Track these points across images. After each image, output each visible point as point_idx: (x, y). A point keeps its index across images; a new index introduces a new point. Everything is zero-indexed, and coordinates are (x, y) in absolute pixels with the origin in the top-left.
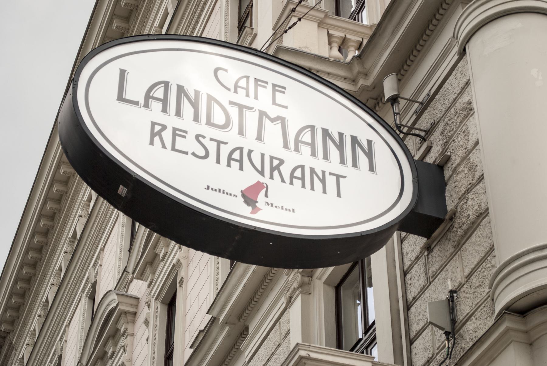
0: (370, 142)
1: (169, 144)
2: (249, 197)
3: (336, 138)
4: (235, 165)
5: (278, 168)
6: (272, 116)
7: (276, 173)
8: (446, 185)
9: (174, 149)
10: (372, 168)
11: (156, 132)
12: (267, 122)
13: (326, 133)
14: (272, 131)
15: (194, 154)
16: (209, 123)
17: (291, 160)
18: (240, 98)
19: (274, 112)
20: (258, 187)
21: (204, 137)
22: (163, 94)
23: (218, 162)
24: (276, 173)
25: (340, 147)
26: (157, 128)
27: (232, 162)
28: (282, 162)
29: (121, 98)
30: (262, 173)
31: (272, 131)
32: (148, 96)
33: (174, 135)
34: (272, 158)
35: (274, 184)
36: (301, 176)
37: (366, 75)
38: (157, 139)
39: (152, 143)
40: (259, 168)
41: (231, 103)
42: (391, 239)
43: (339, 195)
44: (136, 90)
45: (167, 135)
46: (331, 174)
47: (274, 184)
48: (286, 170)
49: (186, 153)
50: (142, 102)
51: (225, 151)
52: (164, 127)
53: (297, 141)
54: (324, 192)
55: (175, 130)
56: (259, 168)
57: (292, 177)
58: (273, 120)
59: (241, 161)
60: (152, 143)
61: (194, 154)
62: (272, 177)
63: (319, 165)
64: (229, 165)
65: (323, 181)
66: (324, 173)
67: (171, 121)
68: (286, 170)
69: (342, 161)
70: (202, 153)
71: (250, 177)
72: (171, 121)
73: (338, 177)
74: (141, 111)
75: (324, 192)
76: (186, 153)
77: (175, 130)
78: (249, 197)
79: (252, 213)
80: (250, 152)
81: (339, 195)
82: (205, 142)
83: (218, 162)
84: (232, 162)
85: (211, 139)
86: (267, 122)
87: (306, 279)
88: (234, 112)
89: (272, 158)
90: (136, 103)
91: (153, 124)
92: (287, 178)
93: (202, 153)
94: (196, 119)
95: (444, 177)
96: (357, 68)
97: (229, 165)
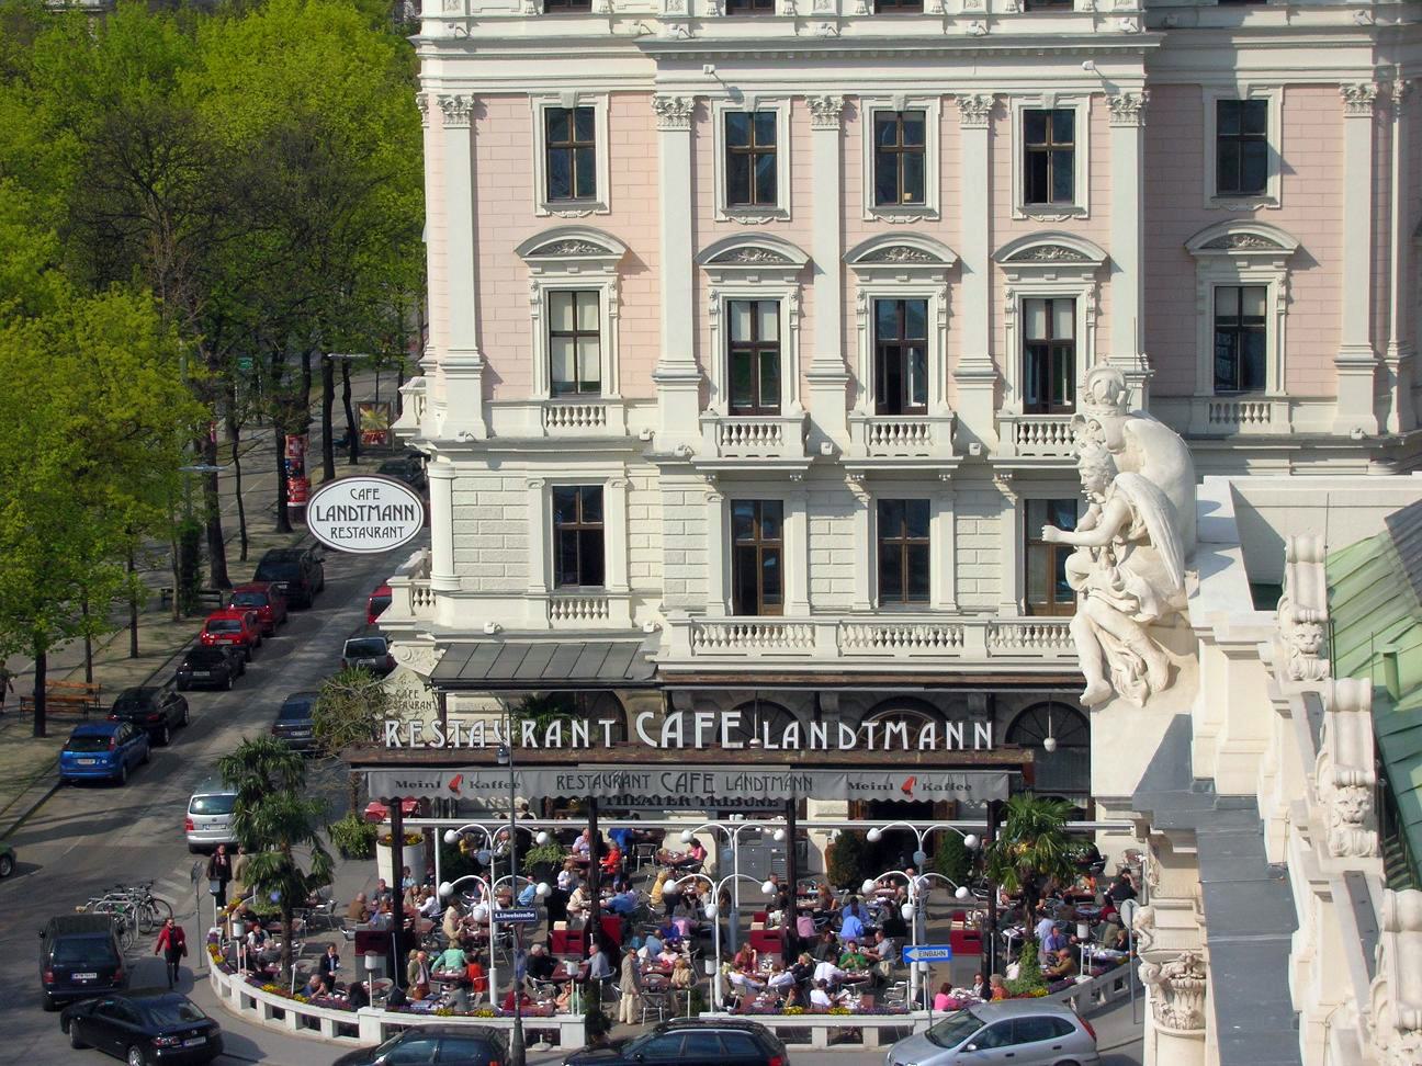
9: (701, 422)
14: (374, 513)
31: (374, 513)
44: (323, 516)
45: (565, 781)
67: (337, 524)
72: (337, 524)
88: (359, 510)
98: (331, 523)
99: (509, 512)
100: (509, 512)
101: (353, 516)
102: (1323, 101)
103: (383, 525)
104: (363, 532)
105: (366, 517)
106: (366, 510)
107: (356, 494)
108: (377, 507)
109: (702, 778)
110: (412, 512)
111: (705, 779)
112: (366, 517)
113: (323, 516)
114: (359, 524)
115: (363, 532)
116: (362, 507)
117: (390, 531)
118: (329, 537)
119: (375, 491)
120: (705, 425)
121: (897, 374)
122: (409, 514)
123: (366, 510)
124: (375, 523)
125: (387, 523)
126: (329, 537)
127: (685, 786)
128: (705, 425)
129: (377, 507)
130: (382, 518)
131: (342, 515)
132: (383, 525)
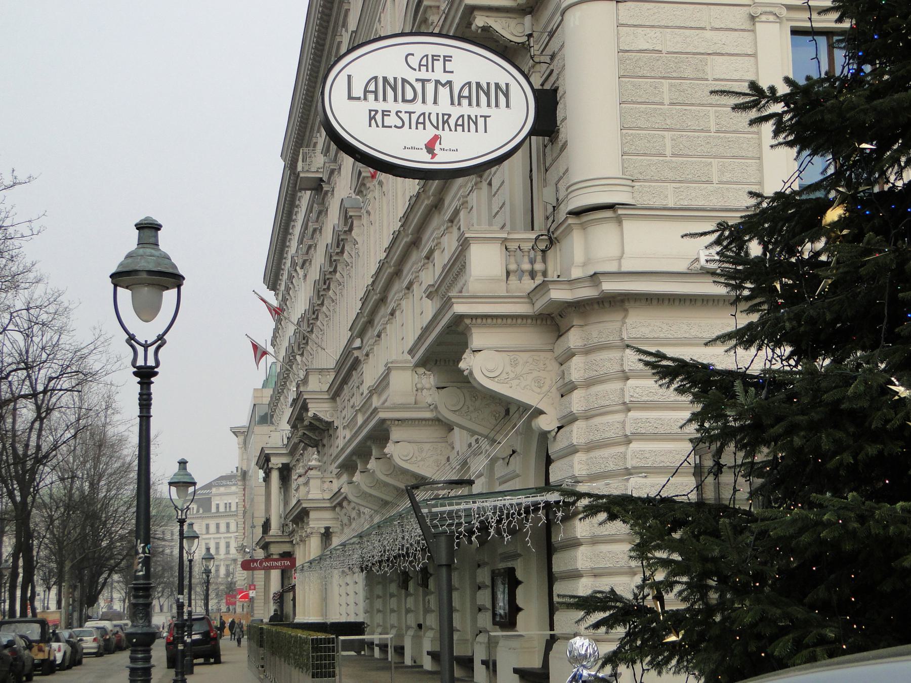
0: (507, 85)
1: (380, 124)
2: (430, 148)
3: (392, 81)
4: (421, 126)
5: (447, 121)
9: (383, 126)
10: (508, 106)
13: (385, 79)
14: (444, 92)
15: (396, 126)
16: (404, 100)
17: (456, 112)
18: (423, 75)
19: (444, 78)
20: (436, 138)
22: (381, 86)
23: (410, 128)
24: (446, 125)
26: (373, 113)
28: (450, 116)
29: (350, 98)
30: (437, 128)
31: (444, 92)
32: (366, 92)
33: (383, 115)
34: (443, 115)
35: (445, 135)
36: (466, 123)
39: (370, 126)
40: (408, 87)
41: (417, 80)
43: (486, 132)
44: (358, 91)
45: (379, 117)
47: (445, 135)
48: (452, 122)
49: (391, 127)
50: (362, 97)
51: (414, 117)
52: (377, 112)
53: (460, 97)
54: (477, 131)
56: (408, 87)
57: (456, 125)
58: (443, 85)
59: (424, 123)
60: (370, 126)
61: (396, 126)
62: (443, 130)
63: (474, 111)
64: (417, 128)
67: (380, 106)
69: (489, 105)
70: (400, 124)
71: (431, 132)
72: (380, 106)
73: (485, 117)
74: (362, 103)
75: (477, 131)
76: (391, 127)
77: (383, 111)
78: (430, 148)
79: (432, 158)
80: (430, 114)
81: (486, 132)
83: (410, 128)
86: (440, 87)
87: (479, 179)
88: (418, 86)
89: (443, 115)
90: (359, 99)
91: (370, 111)
92: (453, 128)
93: (400, 124)
94: (396, 100)
97: (417, 128)
101: (409, 95)
106: (430, 87)
108: (449, 83)
109: (442, 59)
110: (507, 95)
111: (445, 61)
113: (358, 91)
114: (418, 107)
116: (423, 81)
119: (447, 58)
123: (430, 87)
125: (465, 109)
127: (427, 66)
129: (449, 83)
131: (390, 93)
132: (456, 112)
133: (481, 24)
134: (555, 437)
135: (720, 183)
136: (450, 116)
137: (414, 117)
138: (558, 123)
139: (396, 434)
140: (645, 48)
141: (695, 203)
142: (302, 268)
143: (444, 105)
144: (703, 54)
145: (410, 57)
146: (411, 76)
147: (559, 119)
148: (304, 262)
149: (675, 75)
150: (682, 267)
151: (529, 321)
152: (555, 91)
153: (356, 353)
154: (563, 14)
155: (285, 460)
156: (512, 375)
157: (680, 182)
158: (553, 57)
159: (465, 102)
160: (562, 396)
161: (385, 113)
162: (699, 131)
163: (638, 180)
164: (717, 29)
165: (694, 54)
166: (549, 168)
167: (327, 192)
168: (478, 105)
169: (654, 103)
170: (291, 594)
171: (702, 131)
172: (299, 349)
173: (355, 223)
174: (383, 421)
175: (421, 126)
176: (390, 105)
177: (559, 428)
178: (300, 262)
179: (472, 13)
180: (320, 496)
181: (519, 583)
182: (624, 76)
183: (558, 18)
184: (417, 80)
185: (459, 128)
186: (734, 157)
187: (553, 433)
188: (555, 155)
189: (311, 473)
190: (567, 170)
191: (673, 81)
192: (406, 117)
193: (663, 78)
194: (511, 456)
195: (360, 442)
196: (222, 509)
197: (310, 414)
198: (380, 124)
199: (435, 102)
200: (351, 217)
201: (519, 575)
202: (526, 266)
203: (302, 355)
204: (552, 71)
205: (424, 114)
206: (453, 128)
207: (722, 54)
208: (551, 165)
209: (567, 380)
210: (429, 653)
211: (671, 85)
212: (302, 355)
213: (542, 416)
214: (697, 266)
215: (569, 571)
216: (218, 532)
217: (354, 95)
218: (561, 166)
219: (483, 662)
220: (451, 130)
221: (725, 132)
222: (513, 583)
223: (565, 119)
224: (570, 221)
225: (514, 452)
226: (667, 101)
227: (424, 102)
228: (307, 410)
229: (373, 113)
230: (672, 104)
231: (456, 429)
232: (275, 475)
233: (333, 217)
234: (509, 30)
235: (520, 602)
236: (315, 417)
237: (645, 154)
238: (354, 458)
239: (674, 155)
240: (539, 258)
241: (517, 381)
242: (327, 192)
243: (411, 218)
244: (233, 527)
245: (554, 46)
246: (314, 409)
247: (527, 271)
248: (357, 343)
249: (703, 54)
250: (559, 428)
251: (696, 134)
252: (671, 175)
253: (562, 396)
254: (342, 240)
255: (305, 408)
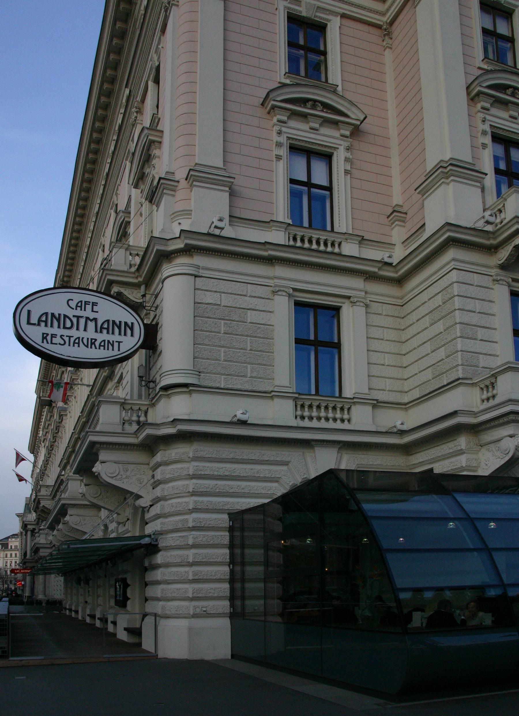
0: (132, 323)
1: (49, 342)
4: (76, 345)
6: (91, 318)
7: (93, 346)
8: (230, 605)
9: (52, 343)
11: (44, 337)
12: (89, 322)
14: (91, 325)
15: (60, 344)
16: (65, 328)
18: (78, 312)
19: (92, 316)
21: (64, 336)
23: (69, 345)
24: (93, 346)
25: (119, 328)
26: (45, 335)
27: (75, 344)
28: (96, 340)
31: (91, 325)
33: (52, 337)
37: (141, 276)
38: (45, 340)
40: (86, 344)
42: (126, 362)
44: (34, 319)
46: (116, 342)
48: (97, 344)
49: (56, 344)
50: (37, 323)
51: (72, 340)
52: (48, 335)
55: (52, 335)
56: (86, 344)
57: (100, 346)
58: (91, 320)
59: (79, 343)
61: (60, 344)
64: (74, 346)
65: (113, 345)
66: (113, 341)
67: (49, 330)
68: (97, 344)
69: (120, 334)
70: (62, 342)
72: (49, 330)
76: (56, 344)
77: (52, 335)
80: (83, 338)
82: (64, 338)
83: (69, 345)
84: (75, 344)
85: (67, 336)
86: (89, 322)
88: (75, 320)
89: (92, 339)
91: (43, 334)
92: (98, 347)
93: (62, 342)
94: (59, 327)
95: (123, 641)
96: (137, 274)
98: (43, 329)
99: (251, 316)
100: (251, 316)
101: (68, 324)
102: (423, 90)
103: (100, 337)
104: (78, 342)
105: (82, 327)
106: (82, 321)
107: (73, 304)
108: (95, 320)
110: (132, 329)
112: (82, 327)
113: (34, 319)
114: (74, 333)
115: (78, 342)
116: (78, 317)
117: (106, 345)
118: (40, 342)
119: (94, 304)
120: (53, 342)
121: (11, 555)
122: (129, 332)
123: (82, 321)
124: (91, 333)
125: (104, 336)
126: (40, 342)
128: (53, 342)
129: (95, 320)
130: (99, 330)
131: (56, 323)
132: (100, 337)
133: (116, 290)
134: (148, 511)
135: (251, 377)
136: (96, 340)
137: (72, 340)
138: (158, 341)
139: (70, 511)
140: (210, 302)
141: (235, 387)
142: (43, 442)
143: (91, 333)
144: (244, 309)
145: (70, 302)
146: (70, 313)
147: (159, 337)
148: (44, 439)
149: (228, 318)
150: (228, 420)
151: (135, 447)
152: (157, 324)
153: (62, 477)
154: (163, 284)
155: (34, 527)
156: (124, 476)
157: (228, 375)
158: (157, 308)
159: (105, 331)
160: (153, 489)
161: (53, 336)
162: (240, 349)
163: (203, 372)
164: (253, 297)
165: (239, 308)
166: (152, 368)
167: (54, 407)
168: (113, 333)
169: (215, 332)
170: (246, 517)
171: (242, 349)
172: (41, 478)
173: (64, 418)
174: (63, 505)
175: (76, 345)
176: (55, 330)
177: (151, 506)
178: (42, 439)
179: (111, 284)
180: (45, 542)
181: (128, 585)
182: (197, 316)
183: (161, 285)
184: (74, 316)
185: (102, 348)
186: (259, 364)
187: (148, 508)
188: (155, 360)
189: (41, 531)
190: (161, 367)
191: (226, 321)
192: (67, 339)
193: (220, 319)
194: (126, 521)
195: (54, 516)
196: (13, 548)
197: (41, 505)
198: (49, 342)
199: (85, 330)
200: (62, 415)
201: (129, 581)
202: (135, 418)
203: (42, 481)
204: (156, 315)
205: (79, 338)
206: (98, 347)
207: (255, 310)
208: (153, 366)
209: (156, 479)
210: (88, 615)
211: (225, 324)
212: (42, 481)
213: (141, 499)
214: (235, 420)
215: (153, 581)
216: (16, 557)
217: (32, 321)
218: (158, 365)
219: (112, 622)
220: (96, 348)
221: (255, 351)
222: (126, 585)
223: (161, 339)
224: (160, 393)
225: (128, 519)
226: (222, 332)
227: (78, 329)
228: (40, 503)
229: (45, 335)
230: (225, 333)
231: (102, 509)
232: (29, 533)
233: (56, 417)
234: (134, 296)
235: (129, 595)
236: (44, 506)
237: (208, 359)
238: (54, 524)
239: (225, 361)
240: (143, 415)
241: (127, 480)
242: (54, 407)
243: (85, 409)
244: (18, 555)
245: (158, 302)
246: (43, 503)
247: (135, 421)
248: (63, 473)
249: (244, 309)
250: (151, 506)
251: (238, 350)
252: (222, 371)
253: (153, 489)
254: (58, 426)
255: (39, 503)
